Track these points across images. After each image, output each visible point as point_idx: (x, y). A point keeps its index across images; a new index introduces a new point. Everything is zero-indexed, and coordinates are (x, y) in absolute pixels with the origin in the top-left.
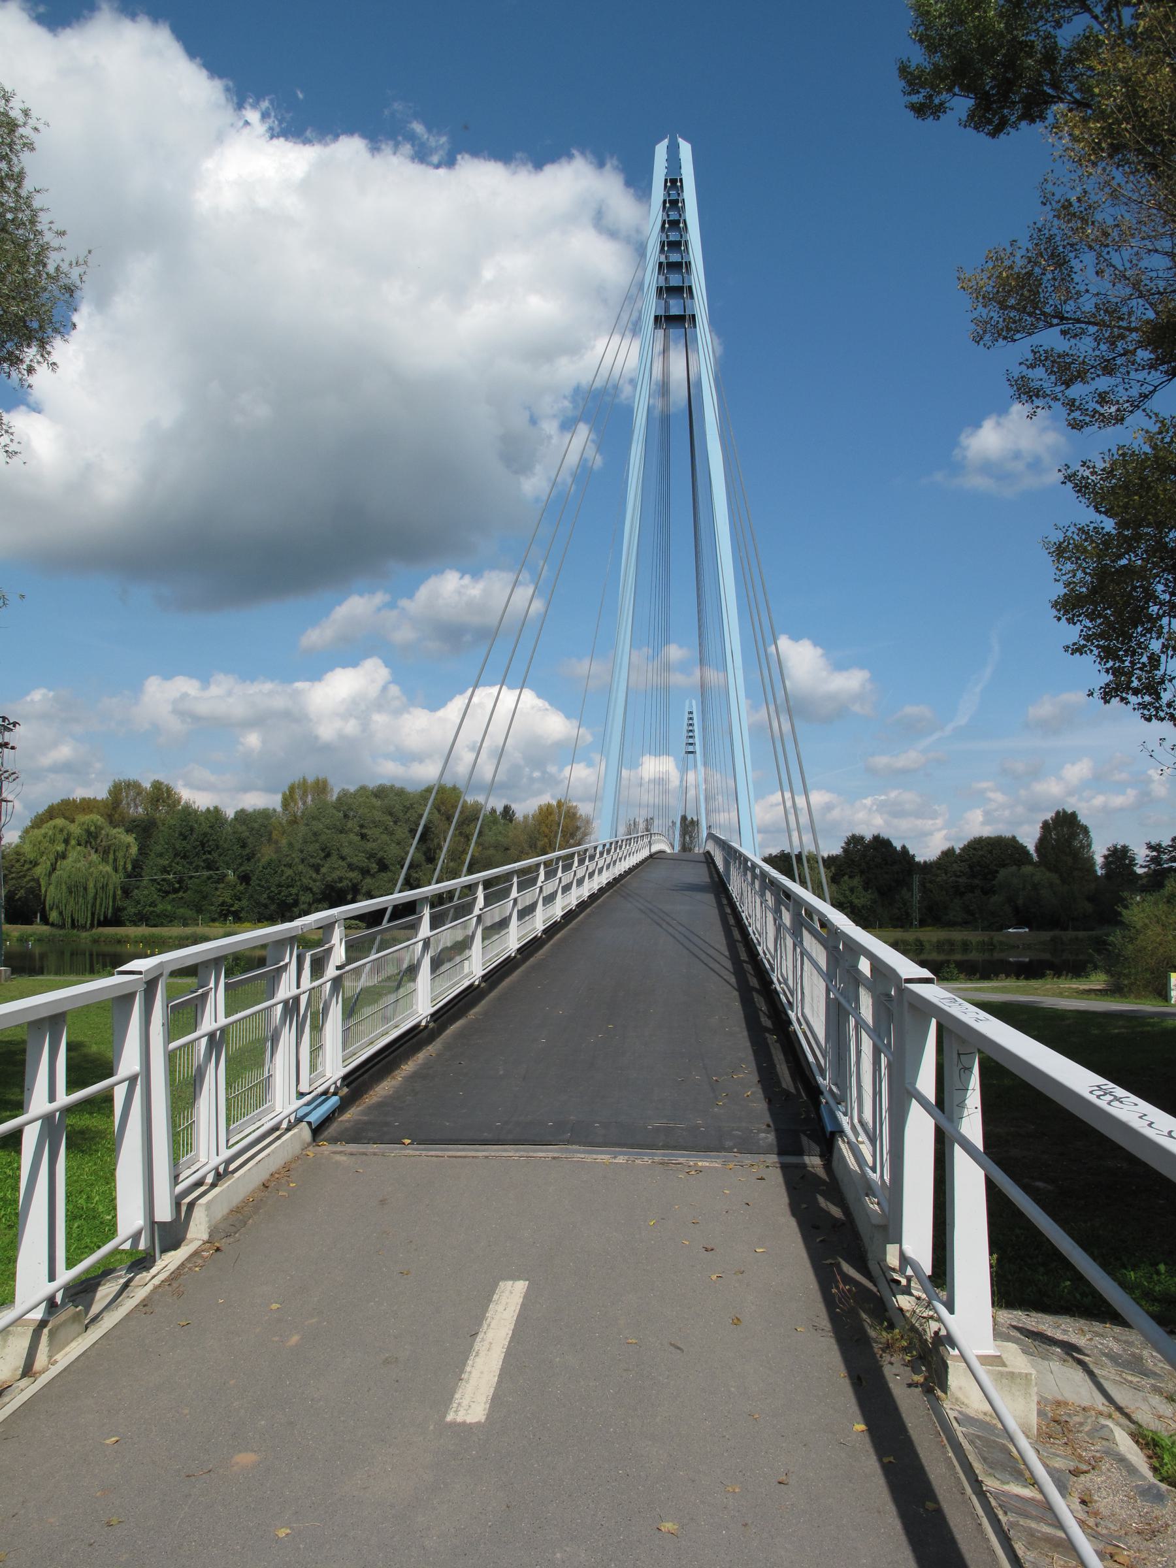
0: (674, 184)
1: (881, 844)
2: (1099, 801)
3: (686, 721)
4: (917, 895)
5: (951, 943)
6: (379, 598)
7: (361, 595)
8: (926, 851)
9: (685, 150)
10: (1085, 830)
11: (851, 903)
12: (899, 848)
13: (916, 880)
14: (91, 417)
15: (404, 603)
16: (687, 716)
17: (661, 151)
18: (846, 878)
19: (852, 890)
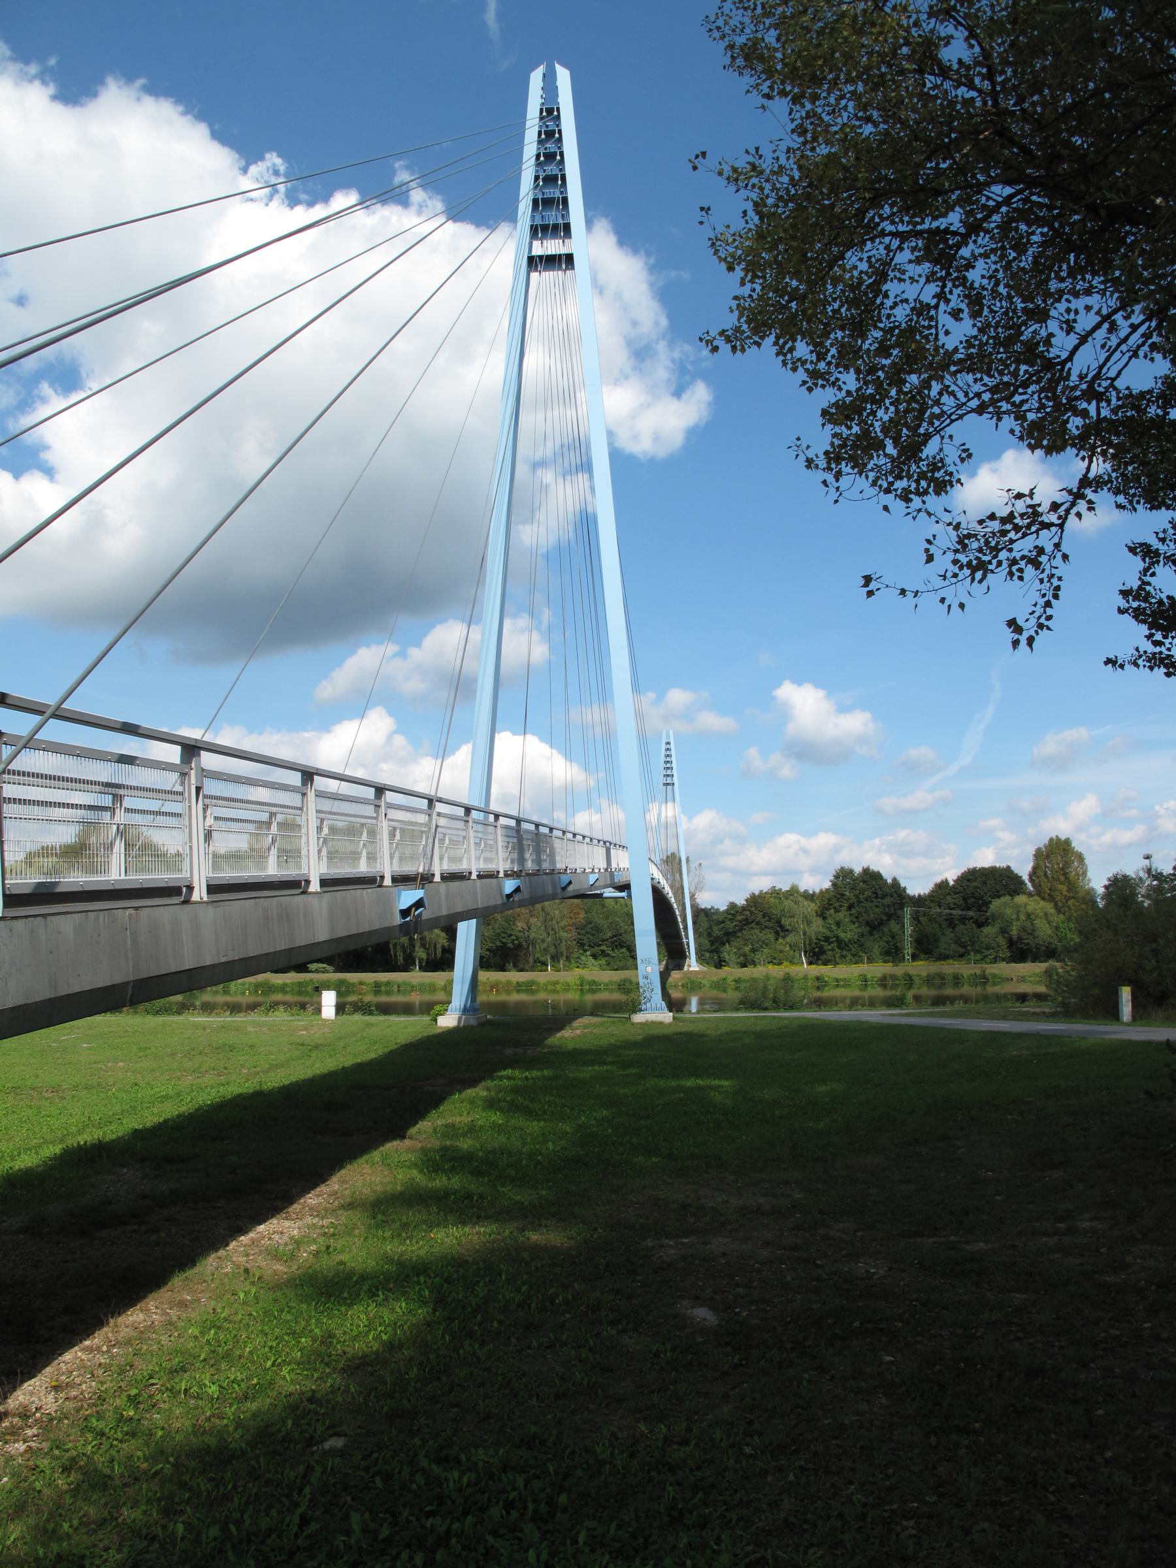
0: (550, 113)
1: (871, 877)
2: (1107, 838)
3: (663, 752)
4: (909, 929)
5: (942, 977)
6: (392, 648)
7: (368, 646)
8: (918, 886)
9: (563, 77)
10: (1080, 857)
11: (838, 937)
12: (889, 881)
13: (908, 911)
14: (106, 484)
15: (415, 653)
16: (664, 746)
17: (536, 79)
18: (832, 911)
19: (838, 924)
